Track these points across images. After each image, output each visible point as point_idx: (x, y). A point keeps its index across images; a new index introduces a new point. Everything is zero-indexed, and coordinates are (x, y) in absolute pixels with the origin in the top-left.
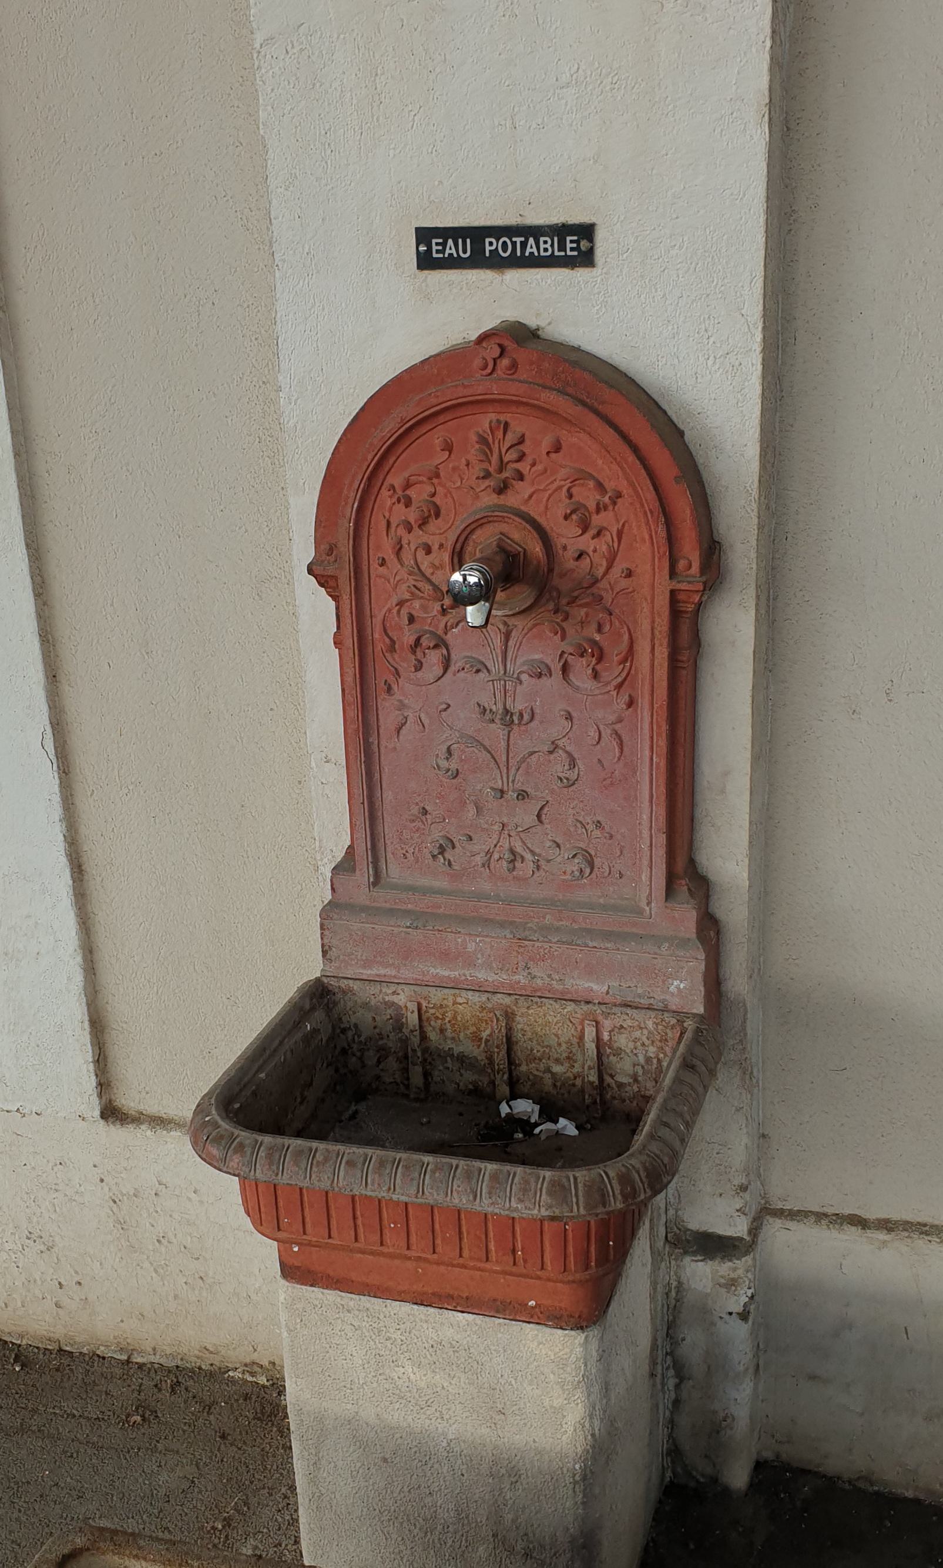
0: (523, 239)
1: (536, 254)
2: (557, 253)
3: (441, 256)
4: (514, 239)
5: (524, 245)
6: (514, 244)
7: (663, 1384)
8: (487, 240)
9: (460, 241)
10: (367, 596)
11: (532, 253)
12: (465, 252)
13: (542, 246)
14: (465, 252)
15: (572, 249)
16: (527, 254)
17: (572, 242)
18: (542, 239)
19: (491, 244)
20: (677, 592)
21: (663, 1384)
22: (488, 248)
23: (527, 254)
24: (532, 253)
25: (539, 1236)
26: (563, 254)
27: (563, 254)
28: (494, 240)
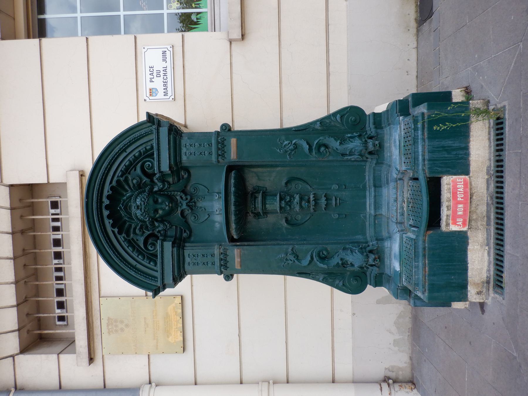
0: (458, 192)
1: (463, 188)
2: (462, 183)
3: (462, 226)
4: (458, 194)
5: (459, 191)
6: (459, 194)
7: (316, 204)
8: (458, 200)
9: (457, 221)
10: (244, 24)
11: (463, 190)
12: (462, 209)
13: (460, 187)
14: (462, 209)
15: (461, 180)
16: (463, 191)
17: (459, 180)
18: (458, 187)
19: (459, 199)
20: (246, 170)
21: (316, 204)
22: (461, 199)
23: (463, 191)
24: (463, 190)
25: (71, 342)
26: (463, 182)
27: (463, 182)
28: (458, 198)
